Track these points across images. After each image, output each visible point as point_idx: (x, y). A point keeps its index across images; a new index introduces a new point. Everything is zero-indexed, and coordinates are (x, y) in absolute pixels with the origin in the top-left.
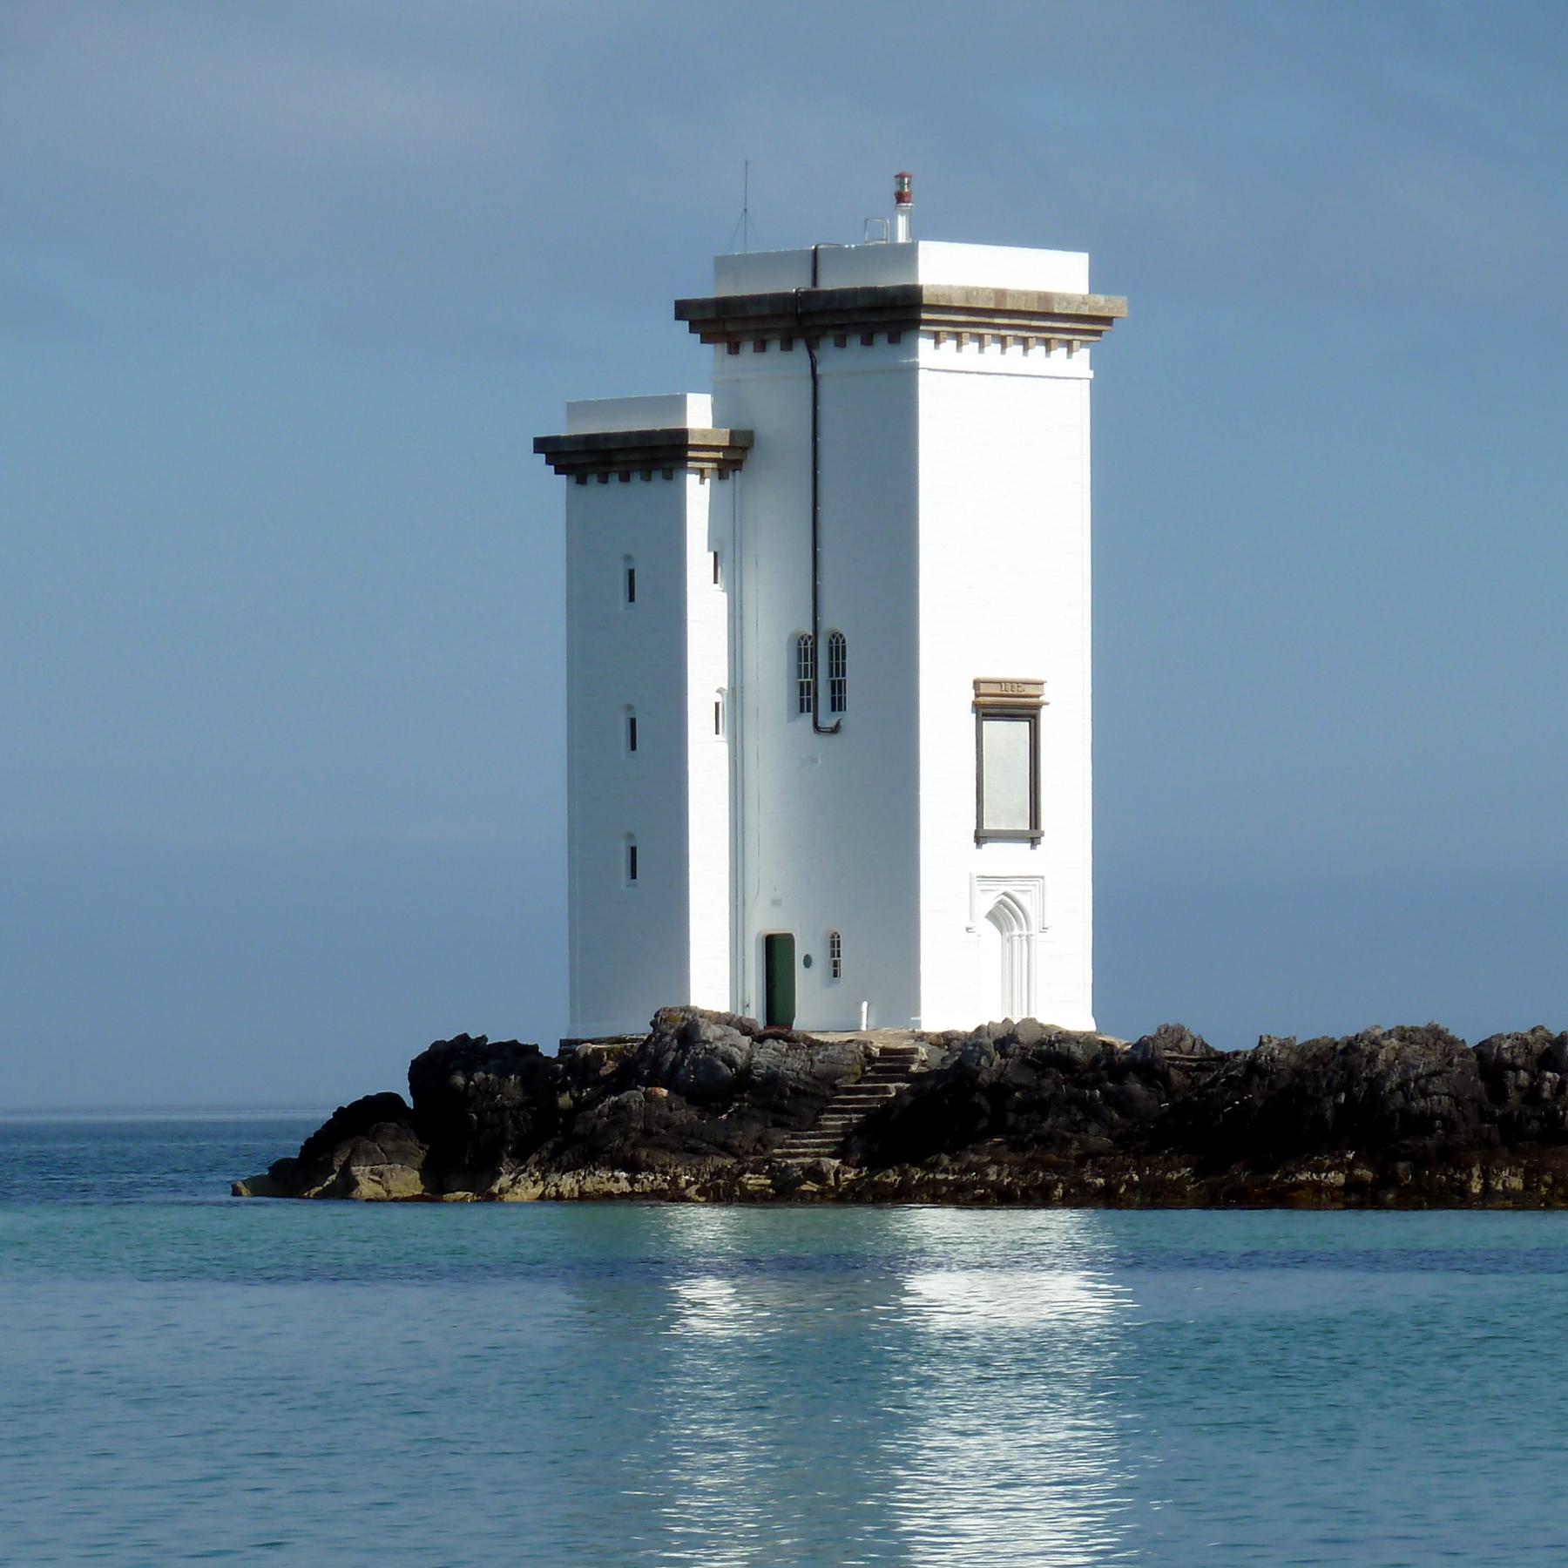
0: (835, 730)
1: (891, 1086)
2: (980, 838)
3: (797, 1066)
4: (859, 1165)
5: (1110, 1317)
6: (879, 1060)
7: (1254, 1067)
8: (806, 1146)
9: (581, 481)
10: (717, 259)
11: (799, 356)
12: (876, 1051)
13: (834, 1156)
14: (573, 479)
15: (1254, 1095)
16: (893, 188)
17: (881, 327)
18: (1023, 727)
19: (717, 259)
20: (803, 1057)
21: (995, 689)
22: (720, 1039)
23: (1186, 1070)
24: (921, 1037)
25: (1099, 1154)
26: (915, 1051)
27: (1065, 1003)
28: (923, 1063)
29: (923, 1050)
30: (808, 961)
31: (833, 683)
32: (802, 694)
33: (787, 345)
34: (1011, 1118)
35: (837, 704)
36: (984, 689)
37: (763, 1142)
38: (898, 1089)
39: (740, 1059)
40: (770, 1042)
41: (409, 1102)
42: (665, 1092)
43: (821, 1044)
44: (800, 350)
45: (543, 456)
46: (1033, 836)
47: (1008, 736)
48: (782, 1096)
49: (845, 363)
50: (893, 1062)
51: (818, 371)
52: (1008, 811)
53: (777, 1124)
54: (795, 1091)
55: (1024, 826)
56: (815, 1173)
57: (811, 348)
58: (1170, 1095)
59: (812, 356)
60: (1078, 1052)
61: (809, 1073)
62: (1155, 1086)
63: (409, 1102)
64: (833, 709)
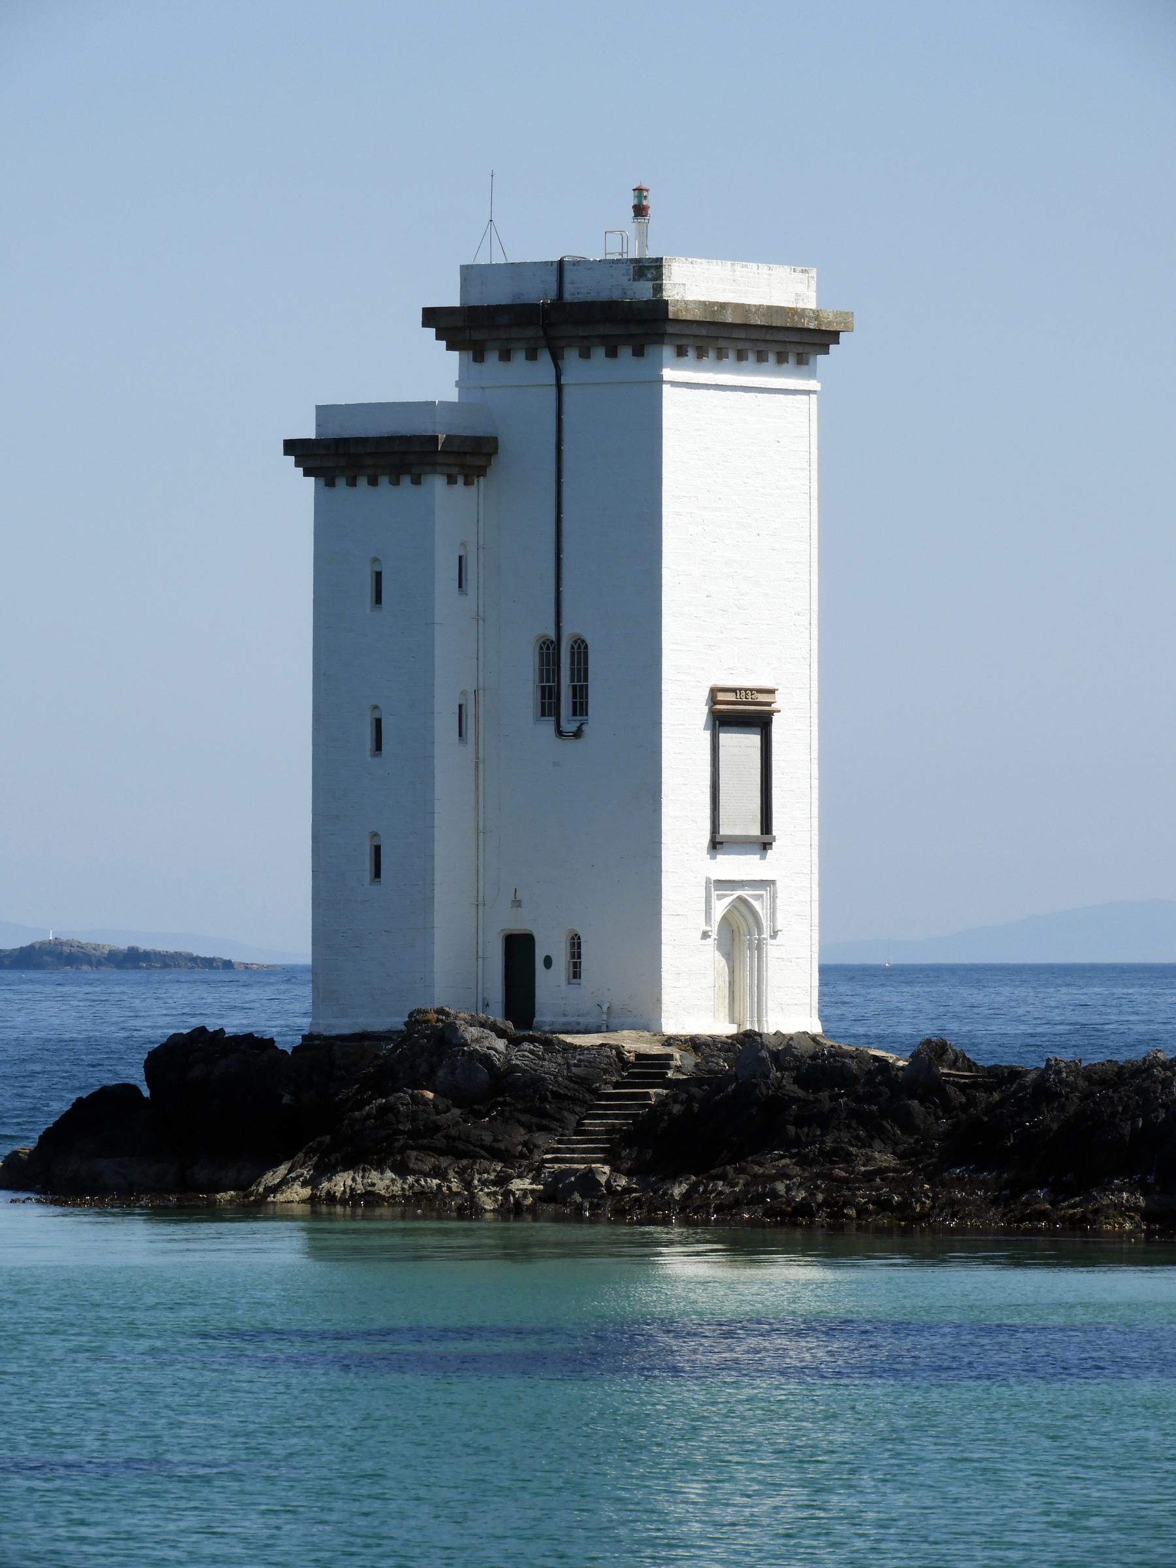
0: (578, 734)
1: (652, 1091)
2: (717, 844)
3: (553, 1068)
4: (629, 1173)
5: (660, 1254)
6: (634, 1065)
7: (1003, 1077)
8: (573, 1151)
9: (330, 483)
10: (462, 267)
11: (544, 366)
12: (632, 1058)
13: (604, 1162)
14: (322, 481)
15: (1049, 1118)
16: (631, 201)
17: (627, 339)
18: (755, 739)
19: (462, 267)
20: (560, 1060)
21: (731, 697)
22: (477, 1040)
23: (963, 1088)
24: (669, 1041)
25: (888, 1170)
26: (670, 1057)
27: (792, 1011)
28: (678, 1069)
29: (677, 1056)
30: (548, 962)
31: (574, 687)
32: (543, 697)
33: (532, 356)
34: (792, 1130)
35: (580, 708)
36: (721, 697)
37: (531, 1147)
38: (657, 1095)
39: (497, 1060)
40: (526, 1045)
41: (146, 1093)
42: (430, 1095)
43: (575, 1048)
44: (545, 358)
45: (444, 343)
46: (764, 842)
47: (741, 746)
48: (543, 1099)
49: (588, 372)
50: (650, 1068)
51: (563, 381)
52: (741, 819)
53: (542, 1128)
54: (555, 1095)
55: (755, 830)
56: (588, 1181)
57: (556, 358)
58: (947, 1107)
59: (557, 366)
60: (853, 1065)
61: (570, 1079)
62: (933, 1102)
63: (146, 1093)
64: (574, 714)
